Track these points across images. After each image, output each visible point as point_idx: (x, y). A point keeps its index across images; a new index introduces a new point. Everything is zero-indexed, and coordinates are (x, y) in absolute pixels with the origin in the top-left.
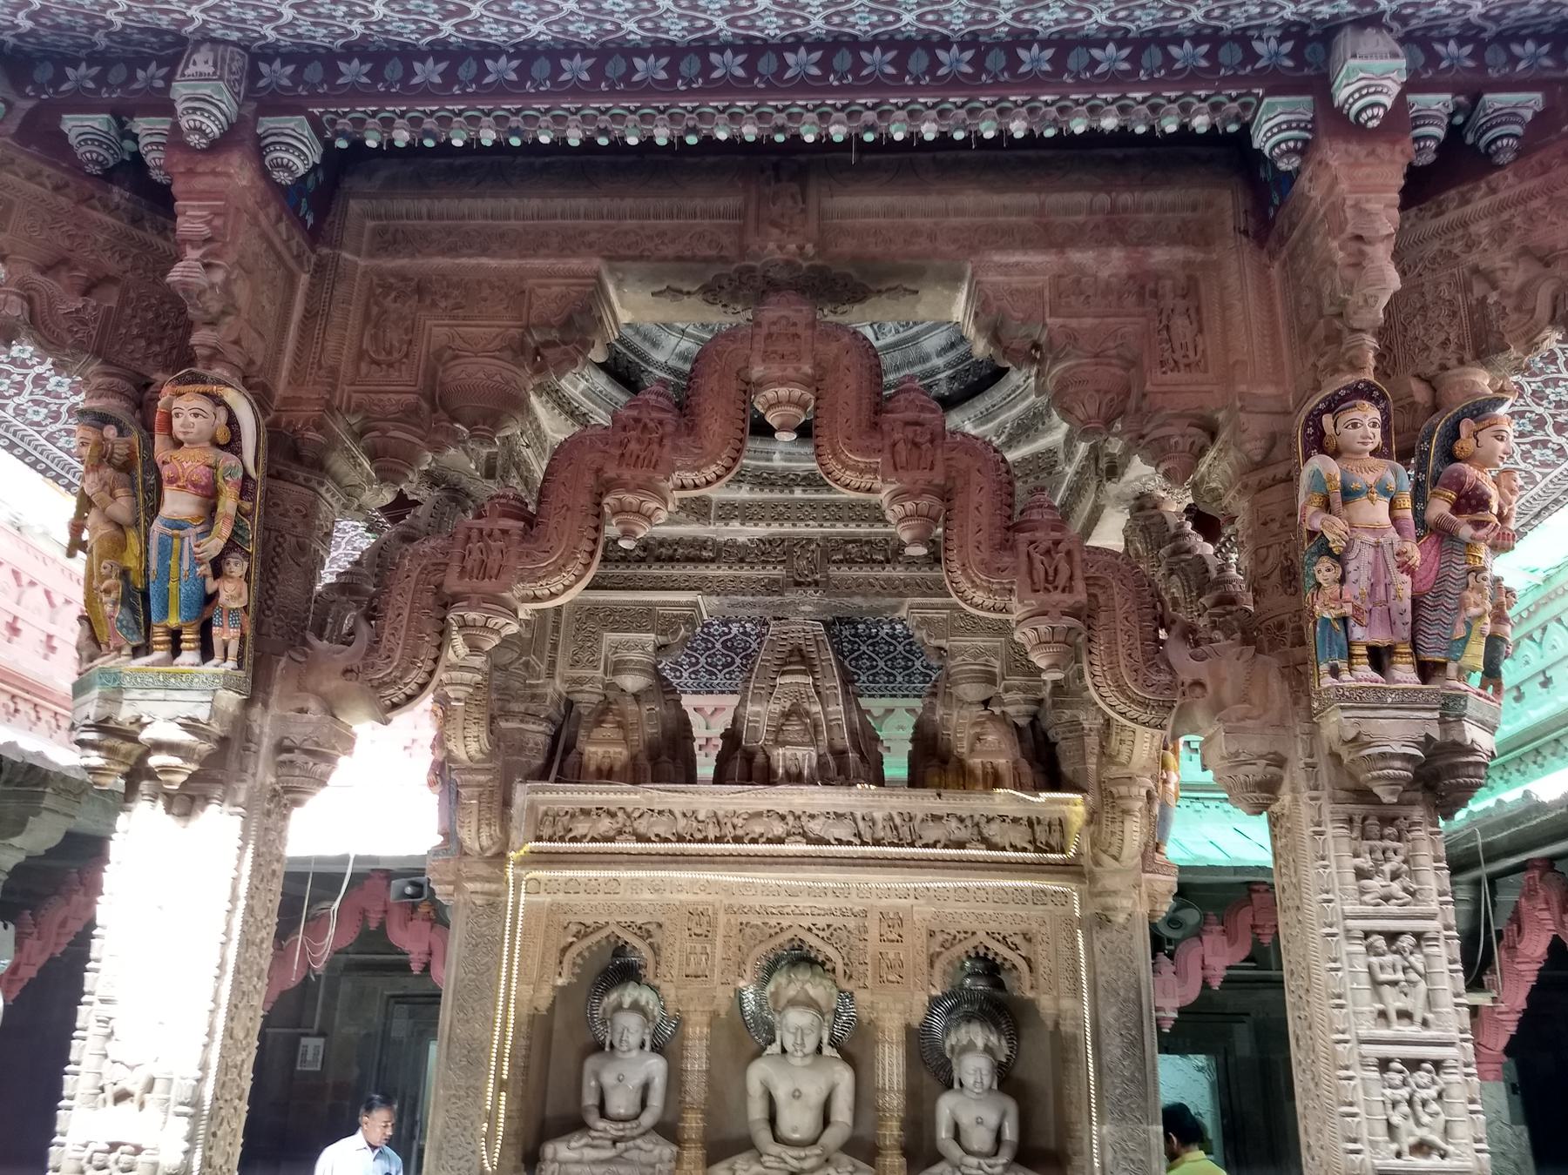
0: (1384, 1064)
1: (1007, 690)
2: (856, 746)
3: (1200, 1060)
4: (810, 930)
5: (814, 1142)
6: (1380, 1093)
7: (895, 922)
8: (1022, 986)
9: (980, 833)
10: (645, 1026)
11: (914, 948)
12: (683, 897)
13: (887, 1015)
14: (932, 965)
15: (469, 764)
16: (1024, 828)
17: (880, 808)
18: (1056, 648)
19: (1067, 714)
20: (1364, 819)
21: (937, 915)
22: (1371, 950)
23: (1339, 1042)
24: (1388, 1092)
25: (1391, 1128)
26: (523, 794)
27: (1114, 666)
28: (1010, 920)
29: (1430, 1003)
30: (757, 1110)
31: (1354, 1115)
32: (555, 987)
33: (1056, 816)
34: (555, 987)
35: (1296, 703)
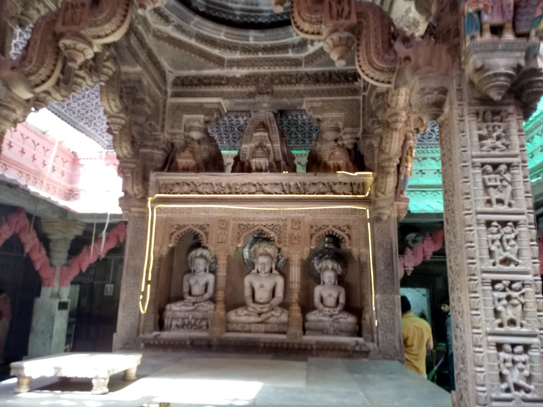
0: (488, 224)
1: (344, 134)
2: (285, 160)
3: (424, 291)
5: (268, 302)
6: (485, 237)
7: (297, 222)
8: (346, 246)
9: (331, 189)
10: (206, 264)
11: (305, 232)
12: (216, 214)
13: (294, 255)
14: (311, 238)
15: (125, 159)
16: (348, 186)
17: (292, 180)
18: (340, 48)
19: (368, 141)
20: (484, 113)
21: (313, 220)
22: (485, 172)
23: (467, 214)
24: (490, 236)
25: (491, 253)
26: (153, 177)
27: (368, 53)
28: (342, 221)
29: (513, 195)
30: (247, 293)
31: (474, 263)
32: (168, 247)
33: (362, 181)
34: (168, 247)
35: (453, 62)
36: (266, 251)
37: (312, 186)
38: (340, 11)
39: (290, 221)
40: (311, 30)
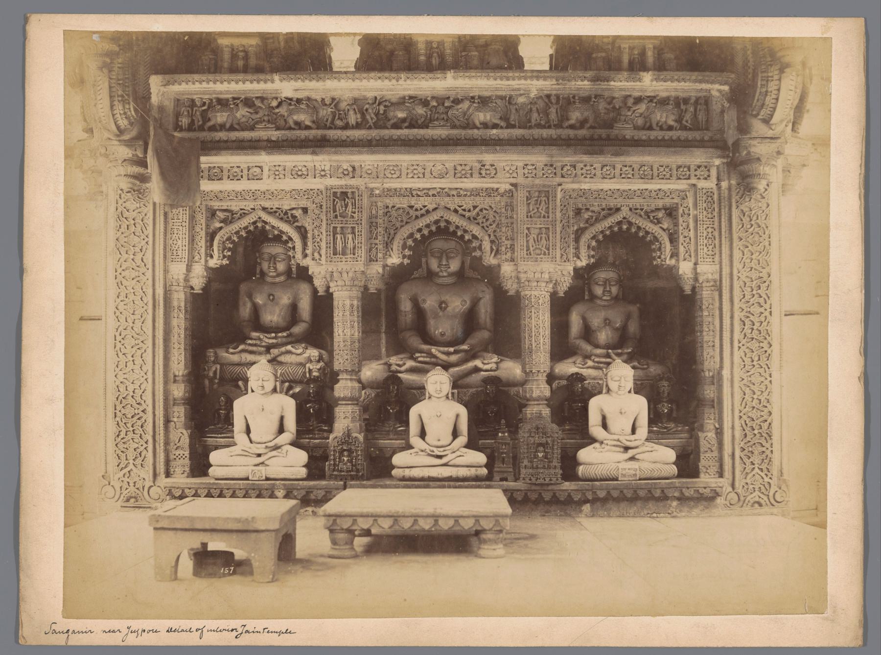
4: (456, 211)
14: (577, 240)
34: (208, 269)
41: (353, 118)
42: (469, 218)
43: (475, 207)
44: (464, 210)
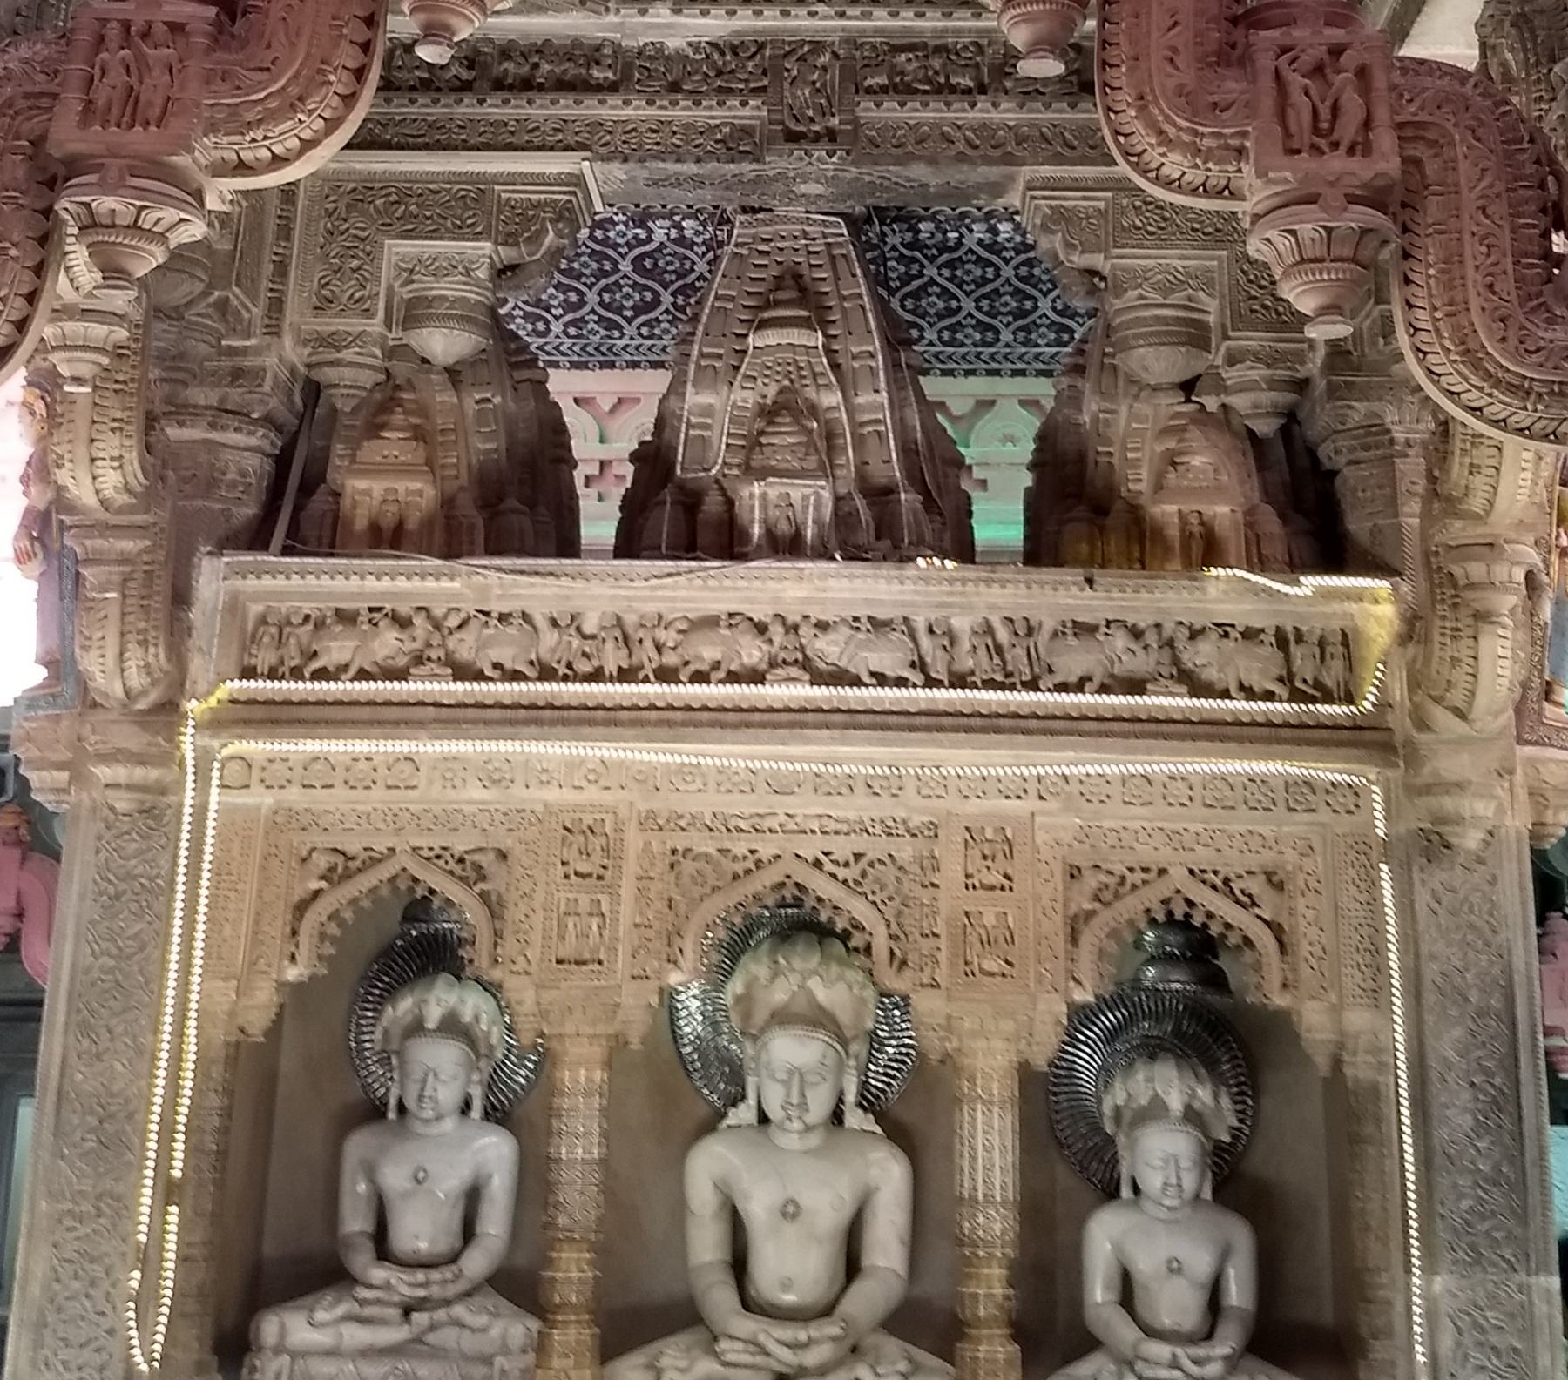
1: (1231, 360)
2: (915, 478)
4: (817, 864)
5: (827, 1311)
7: (997, 847)
8: (1264, 983)
9: (1176, 661)
10: (472, 1067)
11: (1037, 905)
12: (552, 795)
14: (1074, 938)
17: (967, 608)
18: (1335, 272)
19: (1359, 411)
21: (1084, 834)
26: (215, 579)
28: (1237, 843)
30: (706, 1244)
32: (282, 985)
33: (1336, 625)
34: (282, 985)
36: (811, 996)
37: (1072, 641)
38: (1325, 112)
39: (960, 837)
40: (1194, 177)
41: (613, 659)
42: (845, 882)
43: (858, 856)
44: (836, 863)
